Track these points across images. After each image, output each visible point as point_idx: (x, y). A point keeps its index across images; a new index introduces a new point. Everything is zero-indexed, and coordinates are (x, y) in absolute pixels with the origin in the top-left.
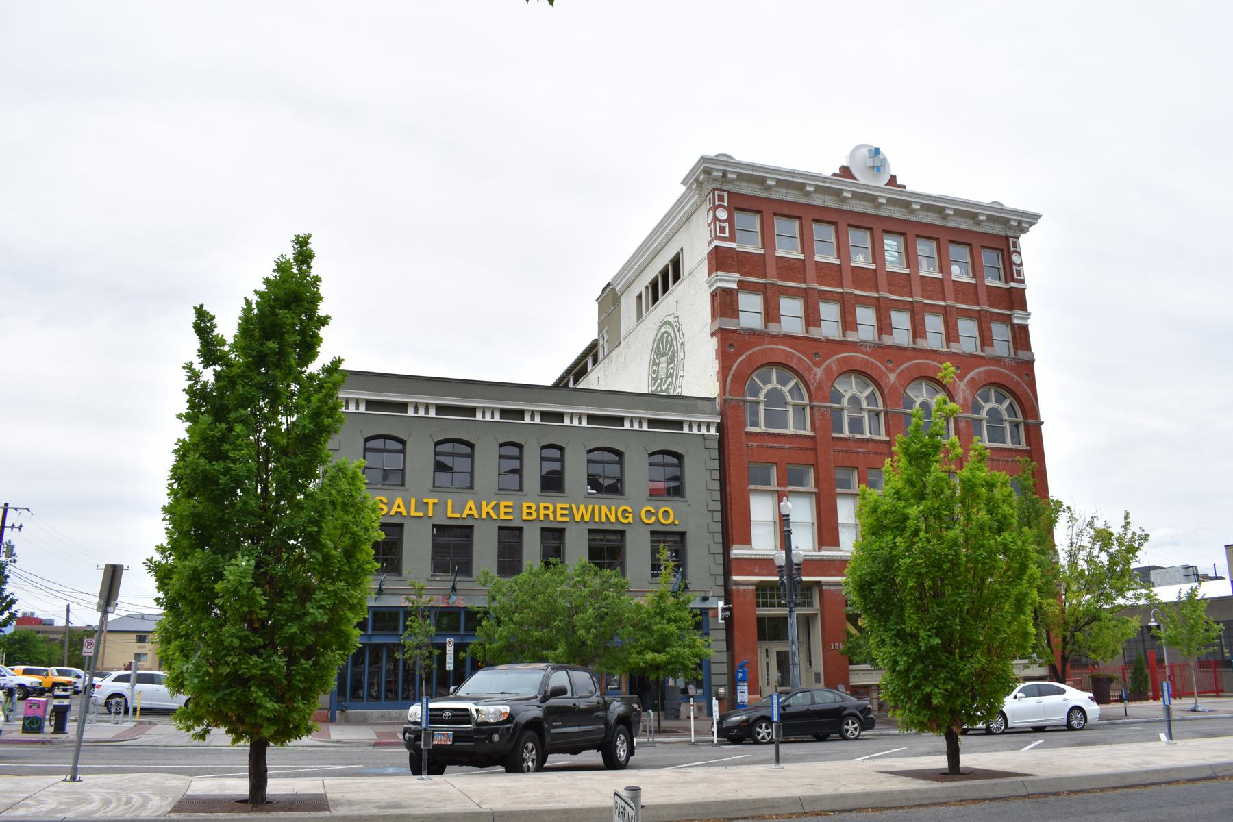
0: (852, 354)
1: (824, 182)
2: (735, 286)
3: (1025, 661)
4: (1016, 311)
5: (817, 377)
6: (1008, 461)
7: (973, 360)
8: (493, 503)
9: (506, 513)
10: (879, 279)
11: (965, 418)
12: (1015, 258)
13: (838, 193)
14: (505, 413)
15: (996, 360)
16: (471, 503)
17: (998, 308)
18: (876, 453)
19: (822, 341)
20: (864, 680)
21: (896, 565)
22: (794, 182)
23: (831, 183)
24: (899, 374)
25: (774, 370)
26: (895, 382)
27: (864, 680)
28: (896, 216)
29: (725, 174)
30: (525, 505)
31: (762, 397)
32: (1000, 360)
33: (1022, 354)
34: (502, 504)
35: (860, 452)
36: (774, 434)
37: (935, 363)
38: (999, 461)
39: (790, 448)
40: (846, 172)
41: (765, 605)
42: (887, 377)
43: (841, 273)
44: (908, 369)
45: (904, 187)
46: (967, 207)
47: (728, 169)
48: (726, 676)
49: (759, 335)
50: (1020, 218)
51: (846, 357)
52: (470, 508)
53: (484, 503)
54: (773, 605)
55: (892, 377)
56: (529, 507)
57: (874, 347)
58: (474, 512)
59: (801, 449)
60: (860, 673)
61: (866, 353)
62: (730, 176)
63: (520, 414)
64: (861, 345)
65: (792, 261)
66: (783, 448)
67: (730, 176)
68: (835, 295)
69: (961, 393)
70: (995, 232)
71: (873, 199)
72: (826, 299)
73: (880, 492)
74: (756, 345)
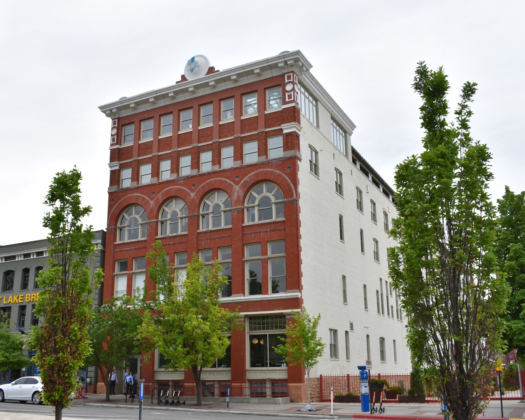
0: (171, 187)
1: (157, 93)
2: (117, 168)
3: (172, 370)
4: (282, 125)
5: (151, 206)
6: (267, 231)
7: (248, 169)
8: (17, 296)
9: (21, 300)
10: (157, 146)
11: (236, 209)
12: (115, 131)
13: (186, 90)
14: (7, 258)
15: (266, 164)
16: (11, 297)
17: (273, 127)
18: (180, 243)
19: (157, 185)
20: (209, 377)
21: (167, 310)
22: (160, 95)
23: (160, 92)
24: (197, 192)
25: (264, 185)
26: (194, 197)
27: (209, 377)
28: (207, 93)
29: (286, 62)
30: (27, 295)
31: (211, 210)
32: (269, 163)
33: (290, 153)
34: (20, 296)
35: (170, 244)
36: (268, 223)
37: (220, 179)
38: (260, 232)
39: (135, 249)
40: (183, 78)
41: (255, 329)
42: (190, 195)
43: (219, 131)
44: (202, 187)
45: (218, 71)
46: (244, 69)
47: (286, 59)
48: (230, 372)
49: (126, 191)
50: (283, 60)
51: (168, 190)
52: (10, 300)
53: (15, 296)
54: (259, 329)
55: (193, 195)
56: (28, 296)
57: (185, 179)
58: (11, 301)
59: (140, 248)
60: (207, 373)
61: (181, 185)
62: (114, 111)
63: (14, 257)
64: (178, 180)
65: (147, 143)
66: (131, 250)
67: (114, 111)
68: (168, 155)
69: (236, 193)
70: (274, 75)
71: (206, 85)
72: (272, 136)
73: (424, 241)
74: (124, 196)
